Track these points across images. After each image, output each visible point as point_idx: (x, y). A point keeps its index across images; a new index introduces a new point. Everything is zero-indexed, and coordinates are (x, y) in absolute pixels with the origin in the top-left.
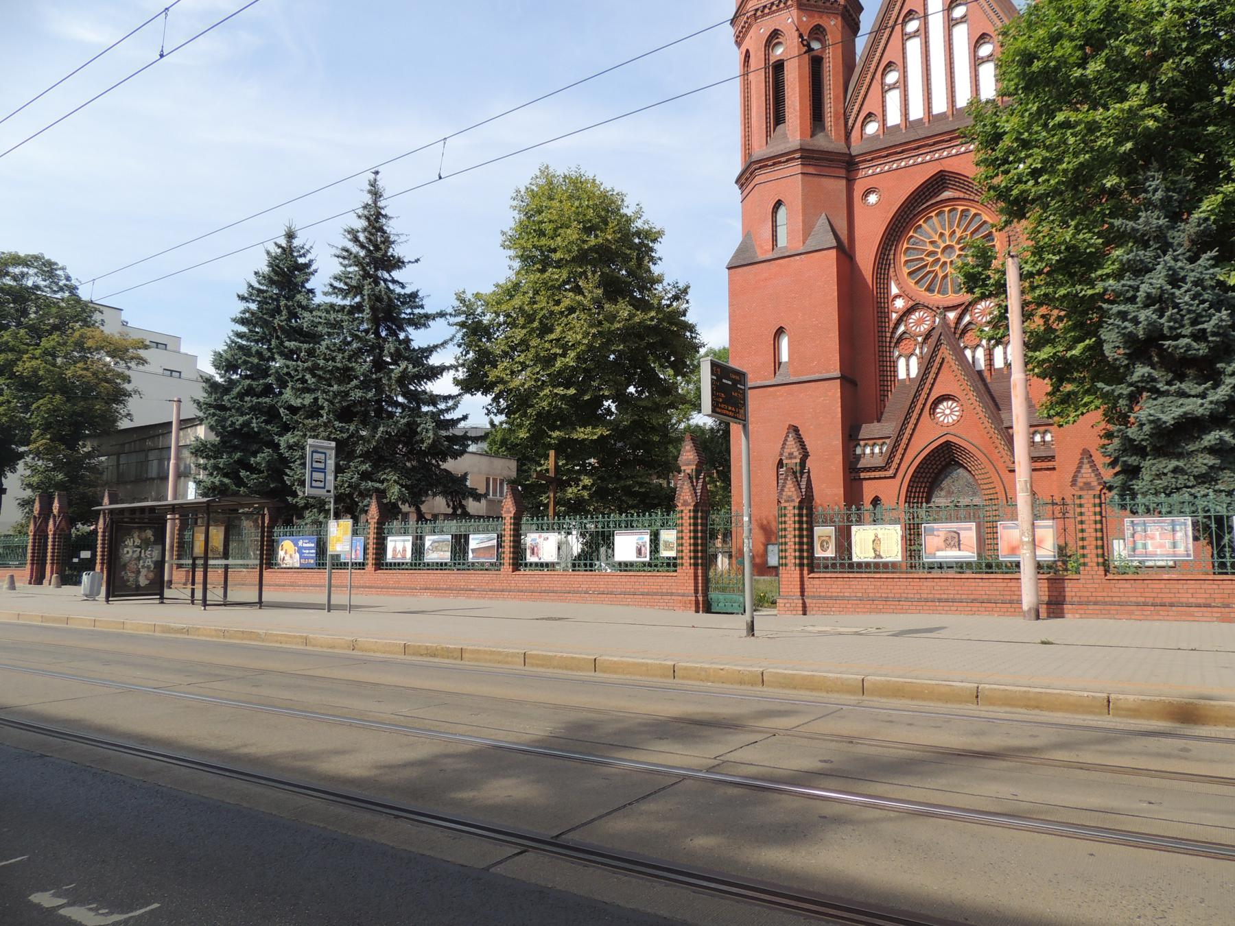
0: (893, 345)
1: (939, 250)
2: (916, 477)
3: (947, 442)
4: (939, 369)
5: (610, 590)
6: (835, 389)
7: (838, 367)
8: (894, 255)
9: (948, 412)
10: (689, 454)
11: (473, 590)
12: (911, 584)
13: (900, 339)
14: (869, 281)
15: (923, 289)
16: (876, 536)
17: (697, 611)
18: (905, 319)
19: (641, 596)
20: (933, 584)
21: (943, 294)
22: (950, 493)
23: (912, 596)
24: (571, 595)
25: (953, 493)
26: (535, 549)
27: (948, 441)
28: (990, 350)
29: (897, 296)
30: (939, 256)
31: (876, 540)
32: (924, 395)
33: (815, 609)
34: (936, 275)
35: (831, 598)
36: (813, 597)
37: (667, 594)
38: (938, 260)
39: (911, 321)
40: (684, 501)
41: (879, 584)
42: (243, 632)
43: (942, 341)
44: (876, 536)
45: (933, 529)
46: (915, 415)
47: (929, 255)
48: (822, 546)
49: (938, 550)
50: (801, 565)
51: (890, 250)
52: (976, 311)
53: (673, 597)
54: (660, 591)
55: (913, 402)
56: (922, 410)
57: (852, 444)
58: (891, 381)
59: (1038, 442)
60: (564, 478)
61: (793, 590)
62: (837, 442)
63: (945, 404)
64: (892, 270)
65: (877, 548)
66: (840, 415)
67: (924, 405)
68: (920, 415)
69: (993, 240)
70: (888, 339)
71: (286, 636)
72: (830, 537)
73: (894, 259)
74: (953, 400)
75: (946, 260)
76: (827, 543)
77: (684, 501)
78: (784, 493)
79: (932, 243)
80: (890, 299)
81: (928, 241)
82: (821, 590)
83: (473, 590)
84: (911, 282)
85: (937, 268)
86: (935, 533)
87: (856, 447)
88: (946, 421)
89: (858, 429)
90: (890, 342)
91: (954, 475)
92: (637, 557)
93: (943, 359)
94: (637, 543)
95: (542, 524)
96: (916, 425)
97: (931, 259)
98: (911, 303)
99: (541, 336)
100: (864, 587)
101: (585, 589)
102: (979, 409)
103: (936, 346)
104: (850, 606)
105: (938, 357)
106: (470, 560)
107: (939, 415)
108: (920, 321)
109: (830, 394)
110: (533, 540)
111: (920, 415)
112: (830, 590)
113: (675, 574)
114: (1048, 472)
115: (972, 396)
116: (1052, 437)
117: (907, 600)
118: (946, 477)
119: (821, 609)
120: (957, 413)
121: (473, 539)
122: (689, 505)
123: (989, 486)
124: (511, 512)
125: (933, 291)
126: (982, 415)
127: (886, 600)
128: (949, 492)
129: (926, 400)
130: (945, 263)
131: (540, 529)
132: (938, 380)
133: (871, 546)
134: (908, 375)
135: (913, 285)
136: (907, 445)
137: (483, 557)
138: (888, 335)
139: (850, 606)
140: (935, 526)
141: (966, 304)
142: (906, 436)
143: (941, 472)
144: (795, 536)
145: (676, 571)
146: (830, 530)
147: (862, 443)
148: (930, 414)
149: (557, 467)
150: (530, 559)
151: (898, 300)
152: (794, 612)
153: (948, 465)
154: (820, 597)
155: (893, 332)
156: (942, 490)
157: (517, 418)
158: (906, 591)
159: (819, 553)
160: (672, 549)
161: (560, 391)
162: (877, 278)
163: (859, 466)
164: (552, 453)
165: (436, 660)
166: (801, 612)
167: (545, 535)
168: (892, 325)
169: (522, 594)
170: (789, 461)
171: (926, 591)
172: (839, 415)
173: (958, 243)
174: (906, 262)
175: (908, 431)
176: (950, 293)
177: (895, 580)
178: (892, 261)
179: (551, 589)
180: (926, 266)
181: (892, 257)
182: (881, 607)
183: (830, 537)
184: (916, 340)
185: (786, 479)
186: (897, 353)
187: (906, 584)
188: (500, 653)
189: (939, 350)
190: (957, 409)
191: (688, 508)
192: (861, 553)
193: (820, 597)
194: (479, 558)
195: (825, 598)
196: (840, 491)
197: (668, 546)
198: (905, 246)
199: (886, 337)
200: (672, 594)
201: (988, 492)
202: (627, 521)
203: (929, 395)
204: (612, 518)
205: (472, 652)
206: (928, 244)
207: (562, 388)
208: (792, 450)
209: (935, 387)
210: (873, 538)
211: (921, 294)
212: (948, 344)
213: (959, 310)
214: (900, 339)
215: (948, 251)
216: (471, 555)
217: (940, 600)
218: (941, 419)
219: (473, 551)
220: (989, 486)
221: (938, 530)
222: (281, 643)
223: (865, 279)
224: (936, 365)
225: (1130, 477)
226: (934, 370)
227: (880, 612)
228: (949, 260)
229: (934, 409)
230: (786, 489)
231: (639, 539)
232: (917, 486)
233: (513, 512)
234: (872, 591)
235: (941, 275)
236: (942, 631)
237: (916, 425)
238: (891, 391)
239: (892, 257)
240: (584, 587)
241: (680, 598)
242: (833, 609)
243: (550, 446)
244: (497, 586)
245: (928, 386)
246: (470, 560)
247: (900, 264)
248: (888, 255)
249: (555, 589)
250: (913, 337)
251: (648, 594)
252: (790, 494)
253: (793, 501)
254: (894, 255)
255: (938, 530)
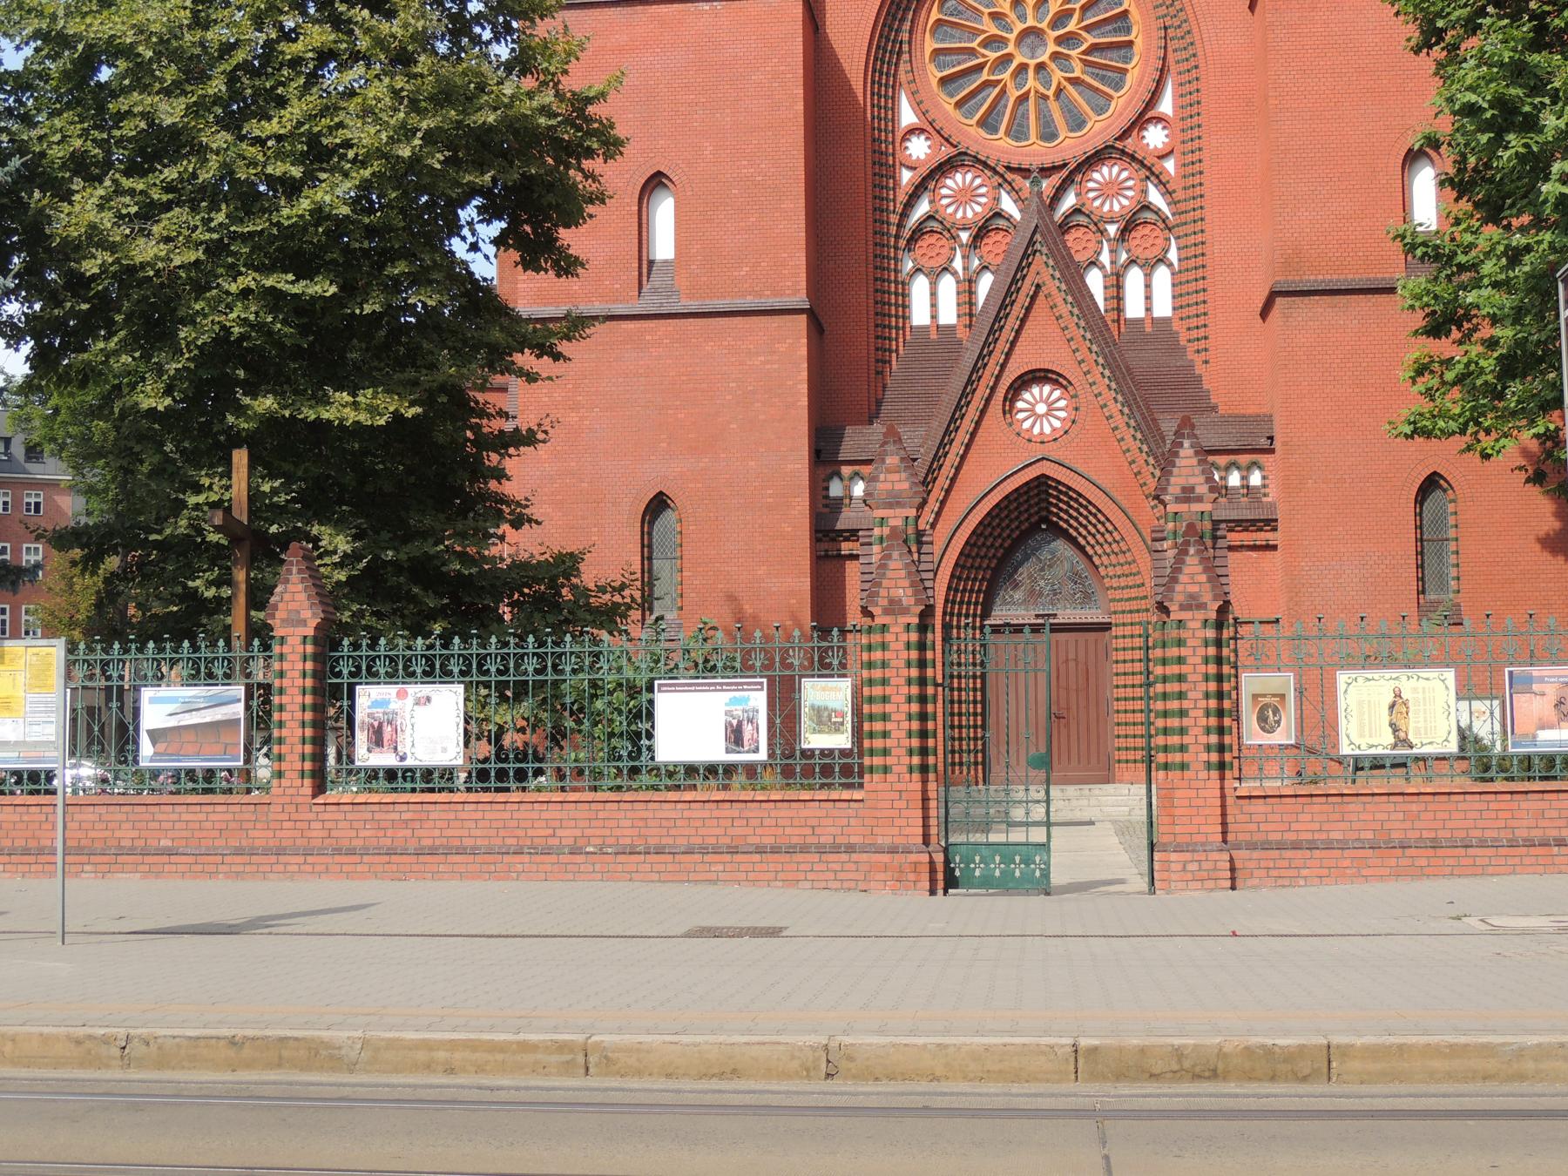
0: (902, 243)
1: (1012, 37)
2: (968, 556)
3: (1042, 480)
4: (1028, 310)
5: (652, 841)
6: (794, 337)
7: (804, 284)
8: (911, 32)
9: (1041, 409)
10: (895, 477)
11: (170, 852)
12: (1492, 806)
13: (918, 233)
14: (857, 84)
15: (973, 121)
16: (1398, 695)
17: (933, 892)
18: (1078, 178)
19: (757, 857)
20: (1541, 805)
21: (1017, 139)
22: (1034, 595)
23: (1495, 835)
24: (526, 858)
25: (1041, 594)
26: (387, 730)
27: (1043, 475)
28: (970, 281)
29: (913, 131)
30: (1010, 48)
31: (1397, 704)
32: (992, 368)
33: (1256, 873)
34: (1003, 92)
35: (1296, 846)
36: (1252, 846)
37: (836, 849)
38: (1008, 58)
39: (944, 191)
40: (892, 602)
41: (1414, 807)
42: (232, 1042)
43: (1038, 246)
44: (1398, 695)
45: (1530, 680)
46: (972, 413)
47: (986, 44)
48: (1262, 719)
49: (1543, 728)
50: (924, 769)
51: (902, 20)
52: (1091, 185)
53: (854, 857)
54: (814, 840)
55: (969, 382)
56: (988, 400)
57: (823, 472)
58: (897, 328)
59: (1234, 488)
60: (274, 529)
61: (1203, 829)
62: (798, 463)
63: (1036, 390)
64: (903, 67)
65: (1401, 724)
66: (804, 401)
67: (993, 389)
68: (983, 412)
69: (1128, 30)
70: (893, 230)
71: (473, 1046)
72: (1282, 697)
73: (910, 43)
74: (1056, 382)
75: (1025, 60)
76: (1276, 711)
77: (892, 602)
78: (1178, 588)
79: (996, 16)
80: (899, 136)
81: (987, 11)
82: (1271, 827)
83: (170, 852)
84: (947, 104)
85: (1006, 76)
86: (1535, 687)
87: (829, 478)
88: (1036, 430)
89: (838, 438)
90: (897, 237)
91: (1045, 555)
92: (728, 751)
93: (1038, 286)
94: (727, 713)
95: (448, 658)
96: (973, 435)
97: (993, 55)
98: (946, 151)
99: (232, 123)
100: (1379, 816)
101: (570, 841)
102: (1114, 408)
103: (1025, 255)
104: (1347, 863)
105: (1028, 281)
106: (143, 764)
107: (1021, 416)
108: (965, 196)
109: (782, 347)
110: (376, 704)
111: (983, 412)
112: (1294, 826)
113: (857, 795)
114: (1254, 554)
115: (1101, 379)
116: (1264, 478)
117: (1482, 844)
118: (1026, 558)
119: (1273, 873)
120: (1062, 414)
121: (152, 701)
122: (905, 611)
123: (1130, 581)
124: (304, 623)
125: (995, 130)
126: (1119, 420)
127: (1435, 845)
128: (1032, 592)
129: (998, 378)
130: (1023, 67)
131: (401, 671)
132: (1024, 334)
133: (1385, 719)
134: (934, 317)
135: (950, 108)
136: (953, 481)
137: (197, 755)
138: (894, 219)
139: (1347, 863)
140: (1536, 671)
141: (1071, 167)
142: (952, 459)
143: (1010, 551)
144: (909, 700)
145: (861, 786)
146: (1284, 681)
147: (846, 470)
148: (1004, 413)
149: (254, 496)
150: (367, 756)
151: (914, 139)
152: (1211, 884)
153: (1035, 528)
154: (1266, 846)
155: (904, 215)
156: (1016, 586)
157: (116, 353)
158: (1481, 824)
159: (1253, 734)
160: (837, 728)
161: (283, 282)
162: (873, 82)
163: (839, 526)
164: (240, 457)
165: (742, 1084)
166: (1228, 884)
167: (415, 690)
168: (902, 197)
169: (357, 859)
170: (1183, 507)
171: (1525, 823)
172: (804, 401)
173: (1055, 24)
174: (937, 52)
175: (956, 449)
176: (1033, 138)
177: (1454, 798)
178: (905, 47)
179: (457, 843)
180: (979, 68)
181: (905, 37)
182: (1424, 862)
183: (1282, 697)
184: (1103, 232)
185: (1183, 552)
186: (910, 264)
187: (1477, 806)
188: (1488, 1050)
189: (1029, 265)
190: (1062, 403)
191: (903, 620)
192: (1362, 735)
193: (1266, 846)
194: (178, 756)
195: (1281, 846)
196: (805, 584)
197: (825, 721)
198: (935, 15)
199: (888, 224)
200: (850, 849)
201: (1126, 594)
202: (467, 660)
203: (1003, 366)
204: (456, 650)
205: (1373, 1052)
206: (986, 18)
207: (290, 277)
208: (1192, 481)
209: (1017, 350)
210: (1390, 698)
211: (973, 136)
212: (1051, 254)
213: (1056, 179)
214: (918, 233)
215: (1029, 41)
216: (146, 748)
217: (1529, 843)
218: (1026, 425)
219: (155, 735)
220: (1130, 581)
221: (1541, 680)
222: (450, 1070)
223: (847, 82)
224: (1022, 299)
225: (437, 562)
226: (1017, 311)
227: (1420, 873)
228: (1032, 63)
229: (1013, 401)
230: (1182, 578)
231: (733, 701)
232: (975, 579)
233: (313, 623)
234: (1397, 825)
235: (1013, 93)
236: (372, 908)
237: (973, 435)
238: (897, 351)
239: (905, 37)
240: (567, 835)
241: (885, 858)
242: (1304, 872)
243: (236, 440)
244: (260, 837)
245: (1002, 346)
246: (143, 764)
247: (923, 55)
248: (898, 31)
249: (468, 842)
250: (949, 231)
251: (775, 850)
252: (1195, 589)
253: (1202, 606)
254: (911, 32)
255: (1541, 680)
